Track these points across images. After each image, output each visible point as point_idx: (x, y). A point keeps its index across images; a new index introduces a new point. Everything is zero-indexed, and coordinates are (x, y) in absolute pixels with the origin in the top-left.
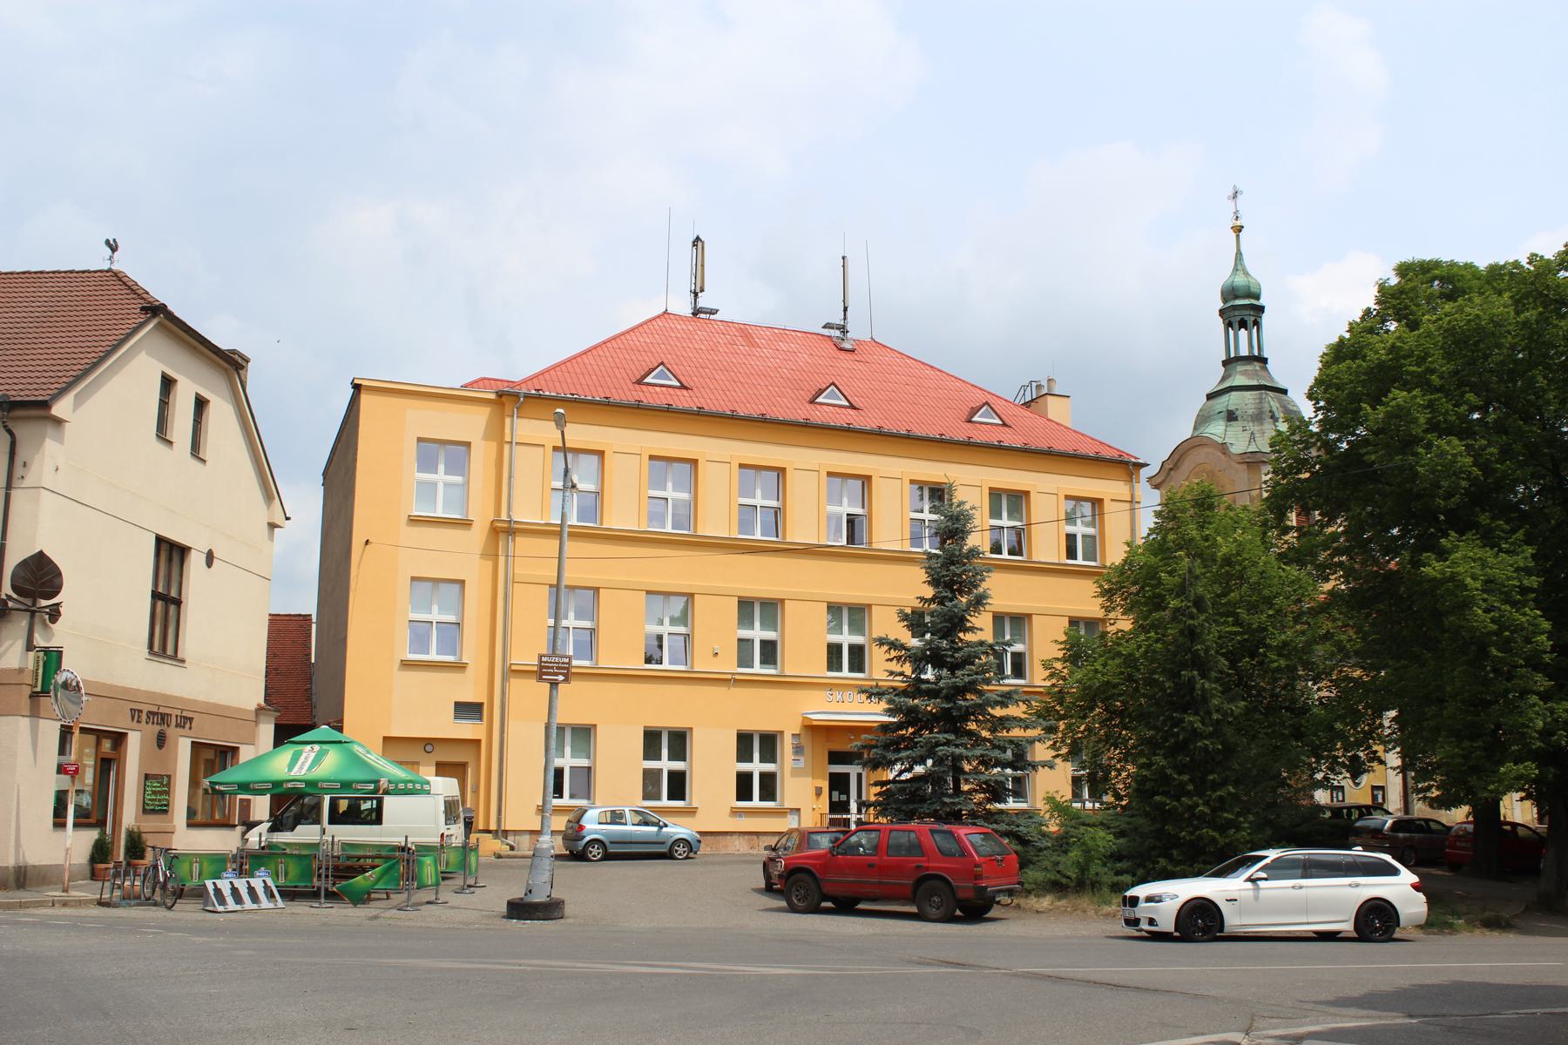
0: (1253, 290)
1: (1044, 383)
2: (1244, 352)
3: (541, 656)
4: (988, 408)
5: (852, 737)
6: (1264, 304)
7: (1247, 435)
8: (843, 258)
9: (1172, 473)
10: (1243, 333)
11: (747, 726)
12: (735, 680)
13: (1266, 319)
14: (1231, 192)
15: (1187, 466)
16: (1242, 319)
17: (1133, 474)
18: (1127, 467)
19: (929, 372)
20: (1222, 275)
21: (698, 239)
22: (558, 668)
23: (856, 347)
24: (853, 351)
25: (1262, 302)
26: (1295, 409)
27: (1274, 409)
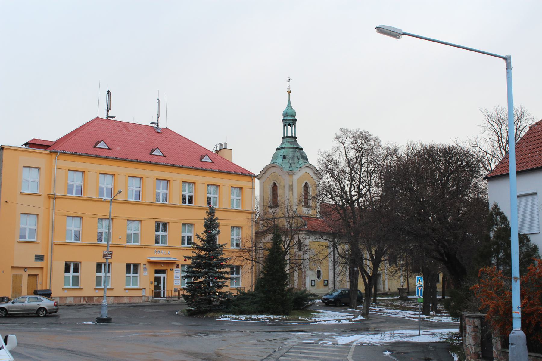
0: (294, 114)
1: (223, 144)
2: (289, 135)
3: (104, 251)
4: (207, 156)
5: (163, 265)
6: (297, 119)
7: (289, 164)
8: (158, 99)
9: (264, 175)
10: (289, 127)
11: (129, 262)
12: (126, 247)
13: (297, 123)
14: (288, 79)
15: (269, 173)
16: (289, 124)
17: (253, 180)
18: (250, 176)
19: (187, 141)
20: (283, 107)
21: (109, 91)
22: (109, 255)
23: (162, 131)
24: (161, 133)
25: (296, 118)
26: (305, 155)
27: (298, 156)
